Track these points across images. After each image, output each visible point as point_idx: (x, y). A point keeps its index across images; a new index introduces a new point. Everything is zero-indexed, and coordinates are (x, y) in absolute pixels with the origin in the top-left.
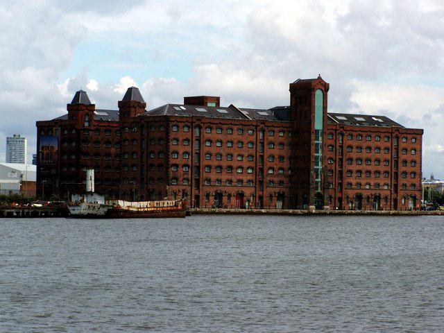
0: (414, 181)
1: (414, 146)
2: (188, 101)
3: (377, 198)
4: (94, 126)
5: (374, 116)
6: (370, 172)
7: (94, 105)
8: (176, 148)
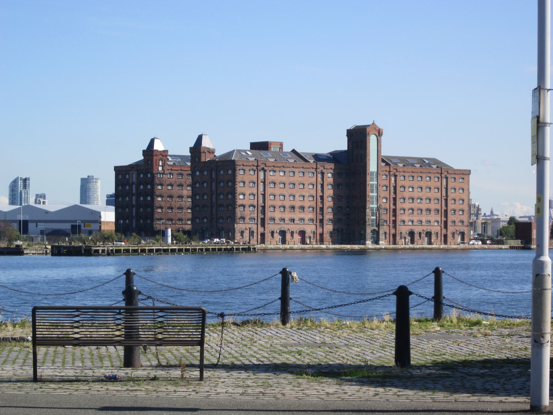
5: (425, 158)
6: (413, 210)
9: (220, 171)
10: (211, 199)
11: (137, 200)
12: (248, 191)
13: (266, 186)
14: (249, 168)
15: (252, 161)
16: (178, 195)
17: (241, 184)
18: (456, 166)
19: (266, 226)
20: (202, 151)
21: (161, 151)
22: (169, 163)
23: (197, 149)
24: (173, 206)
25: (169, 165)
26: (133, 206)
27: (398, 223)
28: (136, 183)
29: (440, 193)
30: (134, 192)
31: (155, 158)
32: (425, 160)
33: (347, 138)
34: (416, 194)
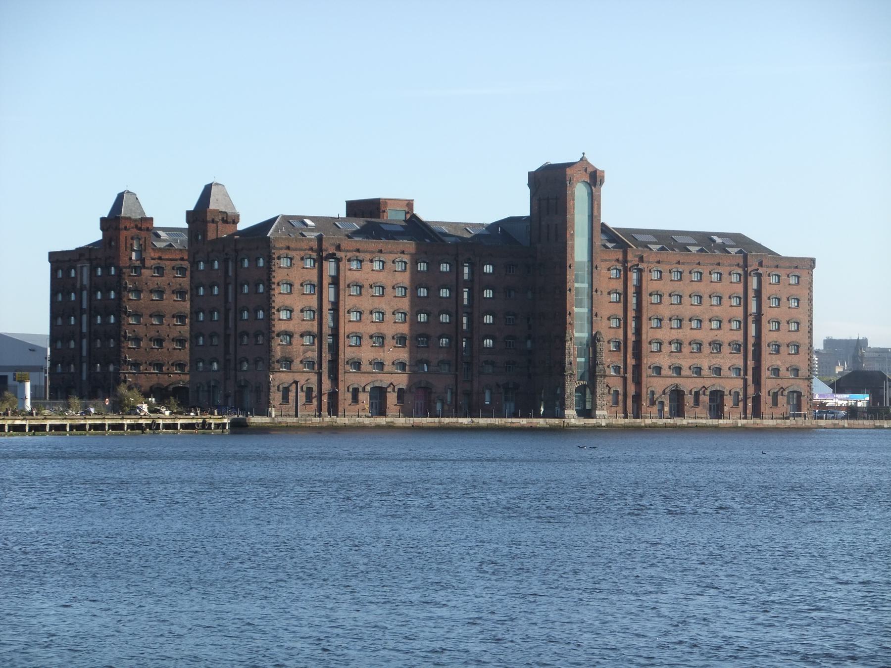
0: (796, 361)
1: (795, 291)
3: (717, 397)
4: (153, 259)
6: (680, 343)
7: (151, 219)
8: (288, 301)
9: (242, 260)
10: (226, 319)
11: (91, 322)
12: (297, 302)
13: (342, 293)
14: (302, 254)
15: (311, 240)
17: (284, 289)
18: (785, 251)
20: (209, 218)
21: (135, 220)
23: (199, 216)
24: (163, 334)
25: (155, 249)
26: (82, 336)
27: (646, 372)
28: (88, 286)
29: (741, 309)
31: (123, 234)
32: (715, 238)
33: (528, 190)
34: (686, 310)
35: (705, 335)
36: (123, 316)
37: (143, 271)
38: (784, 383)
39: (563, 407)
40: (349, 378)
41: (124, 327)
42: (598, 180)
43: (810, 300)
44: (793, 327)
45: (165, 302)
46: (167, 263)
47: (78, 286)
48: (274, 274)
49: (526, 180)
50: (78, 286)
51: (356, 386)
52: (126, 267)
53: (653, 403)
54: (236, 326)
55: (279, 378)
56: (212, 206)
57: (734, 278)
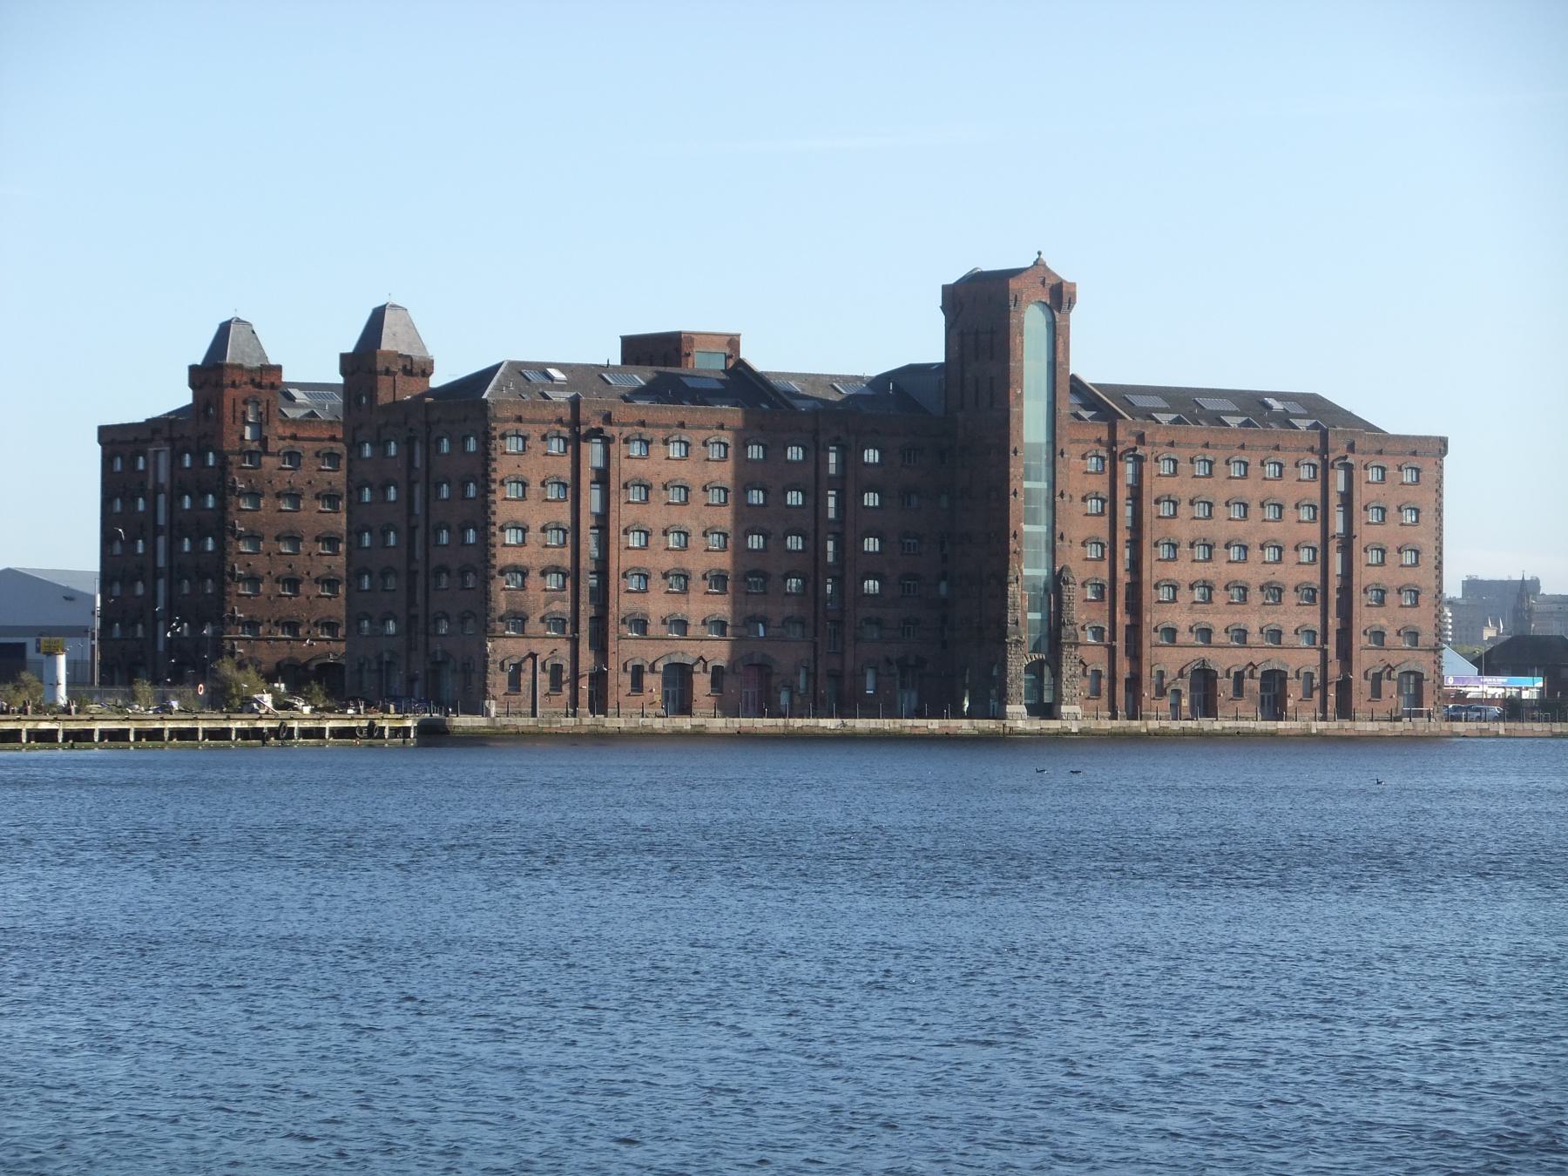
1: (1412, 495)
2: (637, 349)
3: (1274, 682)
4: (283, 438)
6: (1209, 588)
8: (519, 512)
9: (439, 440)
10: (411, 545)
12: (536, 515)
13: (613, 498)
15: (559, 405)
16: (319, 531)
17: (512, 491)
19: (612, 646)
20: (380, 367)
21: (251, 371)
22: (292, 413)
23: (364, 362)
27: (1149, 638)
28: (167, 487)
30: (162, 519)
31: (230, 393)
32: (1271, 401)
34: (1219, 529)
35: (1253, 573)
36: (230, 538)
37: (264, 459)
38: (1393, 658)
39: (1003, 699)
40: (626, 649)
41: (230, 559)
42: (1065, 300)
43: (1439, 511)
44: (1408, 558)
45: (302, 514)
46: (307, 445)
47: (150, 487)
48: (494, 465)
49: (938, 300)
50: (150, 487)
51: (638, 662)
52: (233, 453)
53: (1161, 692)
54: (427, 555)
55: (503, 648)
56: (386, 345)
57: (1305, 473)
